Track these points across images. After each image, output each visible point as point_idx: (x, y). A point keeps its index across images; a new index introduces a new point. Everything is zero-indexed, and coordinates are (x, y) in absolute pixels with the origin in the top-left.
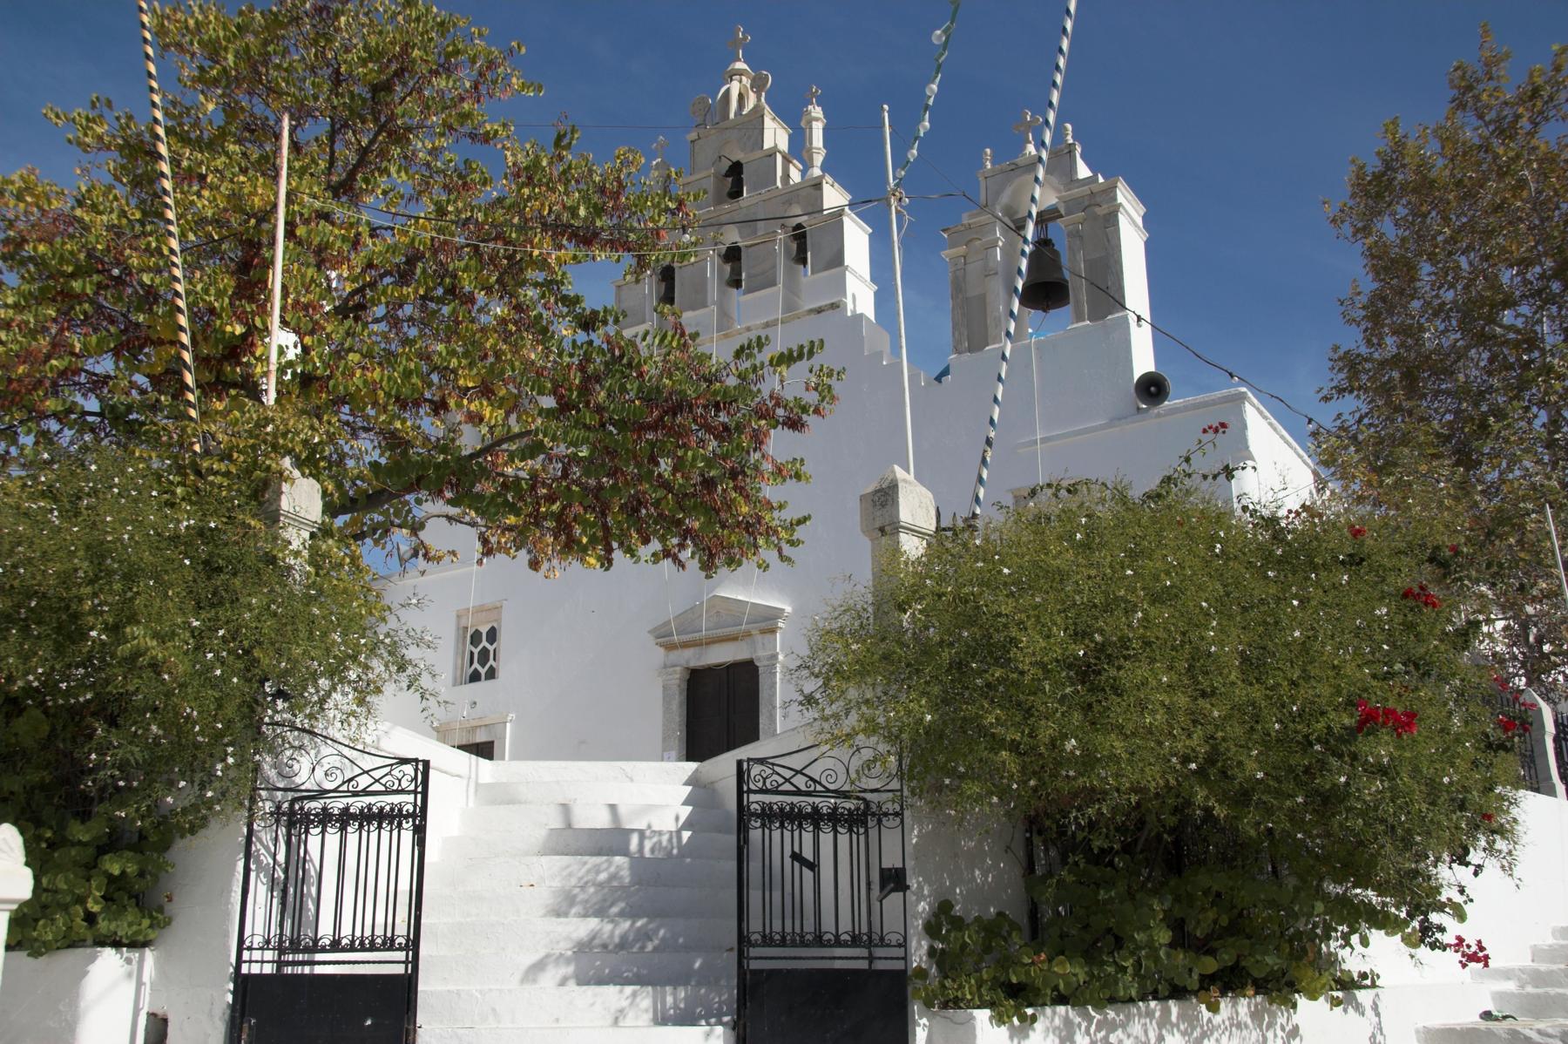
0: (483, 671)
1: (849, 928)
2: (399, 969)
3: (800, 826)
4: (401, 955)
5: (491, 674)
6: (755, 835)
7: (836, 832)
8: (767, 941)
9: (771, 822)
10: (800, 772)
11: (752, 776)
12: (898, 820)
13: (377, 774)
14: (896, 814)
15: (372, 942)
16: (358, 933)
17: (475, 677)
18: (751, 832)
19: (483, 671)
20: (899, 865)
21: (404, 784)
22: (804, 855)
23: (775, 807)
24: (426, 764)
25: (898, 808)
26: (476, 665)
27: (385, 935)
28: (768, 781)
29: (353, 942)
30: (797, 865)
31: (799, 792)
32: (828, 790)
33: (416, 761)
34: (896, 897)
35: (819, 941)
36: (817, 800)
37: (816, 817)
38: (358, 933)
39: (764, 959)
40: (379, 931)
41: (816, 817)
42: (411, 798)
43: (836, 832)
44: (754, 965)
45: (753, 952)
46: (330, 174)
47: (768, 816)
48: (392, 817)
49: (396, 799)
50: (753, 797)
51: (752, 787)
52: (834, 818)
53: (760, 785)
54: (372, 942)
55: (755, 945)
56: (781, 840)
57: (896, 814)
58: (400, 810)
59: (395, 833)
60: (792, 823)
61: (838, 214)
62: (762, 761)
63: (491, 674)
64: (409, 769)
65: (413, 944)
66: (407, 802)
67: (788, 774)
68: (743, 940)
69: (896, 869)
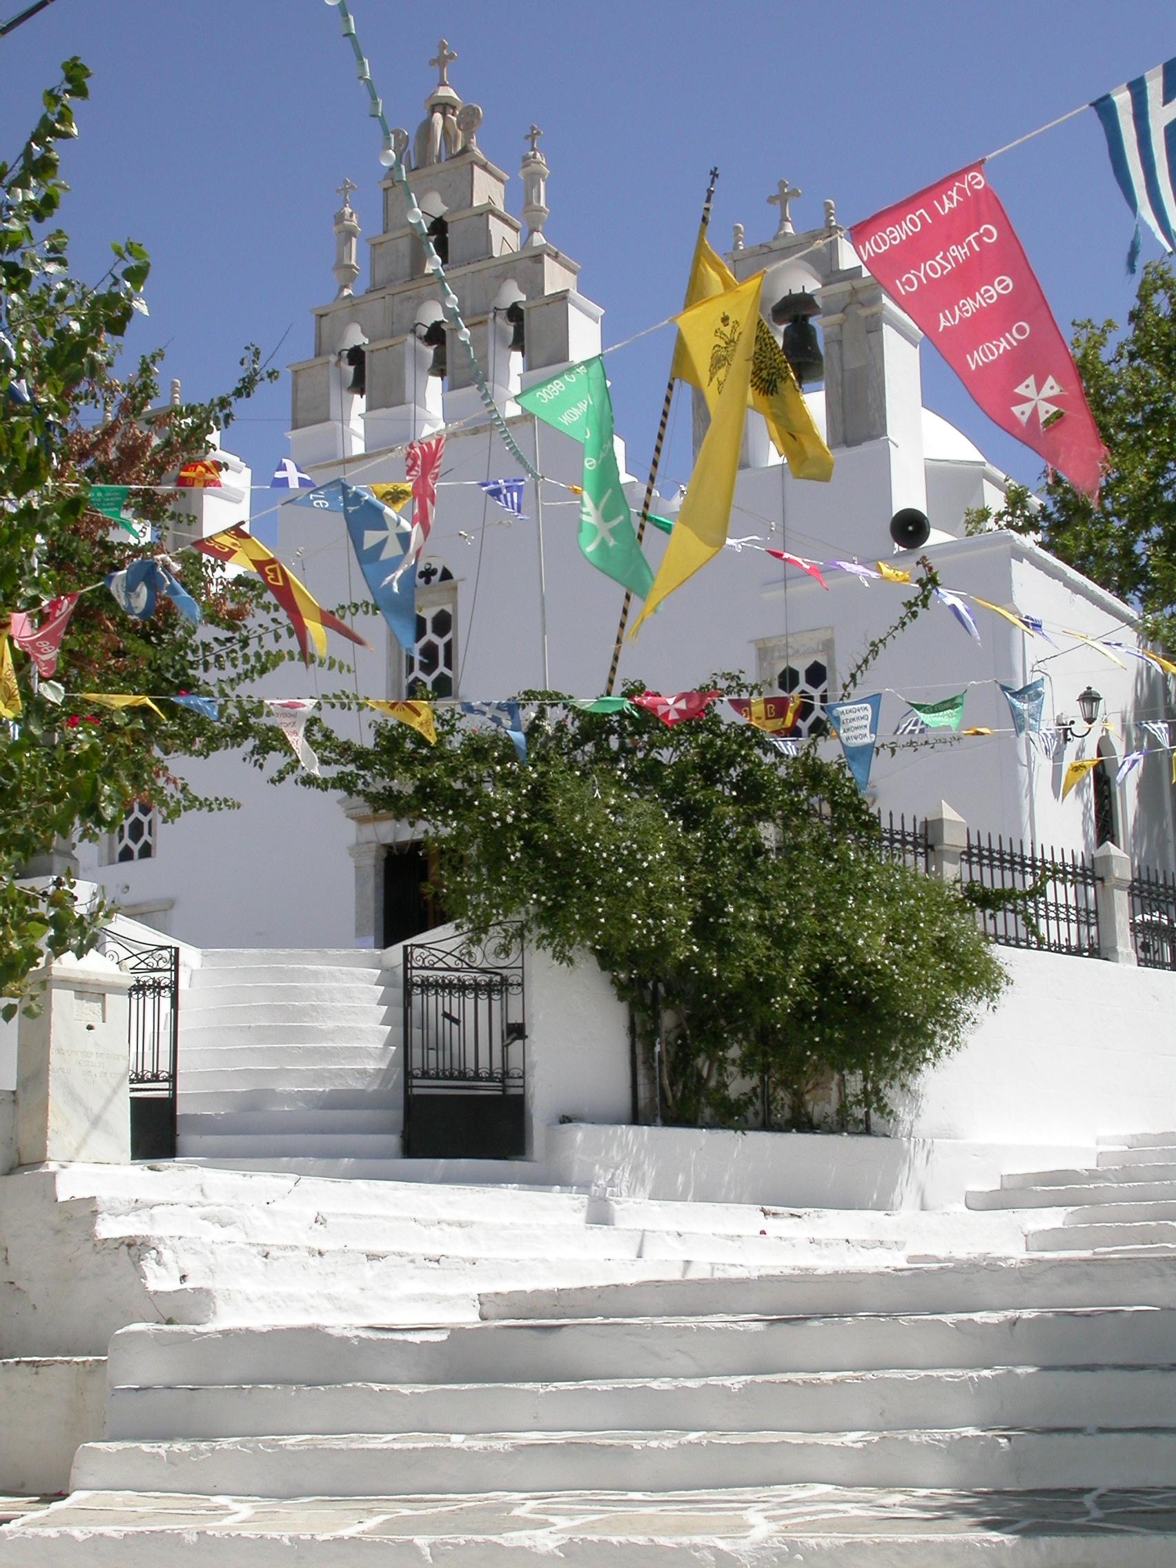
0: (136, 848)
1: (501, 1066)
2: (165, 1094)
3: (450, 993)
4: (166, 1085)
5: (146, 851)
6: (417, 999)
7: (490, 999)
8: (425, 1075)
9: (428, 990)
10: (449, 954)
11: (414, 956)
12: (520, 988)
13: (143, 957)
14: (519, 985)
15: (451, 1074)
16: (441, 1067)
17: (126, 855)
18: (414, 997)
19: (136, 848)
20: (520, 1021)
21: (161, 965)
22: (453, 1014)
23: (431, 979)
24: (177, 949)
25: (520, 981)
26: (127, 841)
27: (437, 1068)
28: (426, 961)
29: (437, 1073)
30: (447, 1021)
31: (449, 969)
32: (471, 967)
33: (170, 947)
34: (519, 1043)
35: (477, 1077)
36: (461, 974)
37: (462, 987)
38: (441, 1067)
39: (421, 1088)
40: (148, 1067)
41: (462, 987)
42: (168, 974)
43: (490, 999)
44: (416, 1091)
45: (415, 1082)
46: (415, 776)
47: (426, 985)
48: (157, 987)
49: (156, 975)
50: (415, 972)
51: (414, 965)
52: (476, 988)
53: (420, 963)
54: (451, 1074)
55: (416, 1078)
56: (435, 1003)
57: (519, 985)
58: (160, 983)
59: (157, 999)
60: (443, 991)
61: (562, 297)
62: (421, 946)
63: (146, 851)
64: (165, 953)
65: (172, 1078)
66: (165, 978)
67: (441, 955)
68: (408, 1074)
69: (518, 1024)
